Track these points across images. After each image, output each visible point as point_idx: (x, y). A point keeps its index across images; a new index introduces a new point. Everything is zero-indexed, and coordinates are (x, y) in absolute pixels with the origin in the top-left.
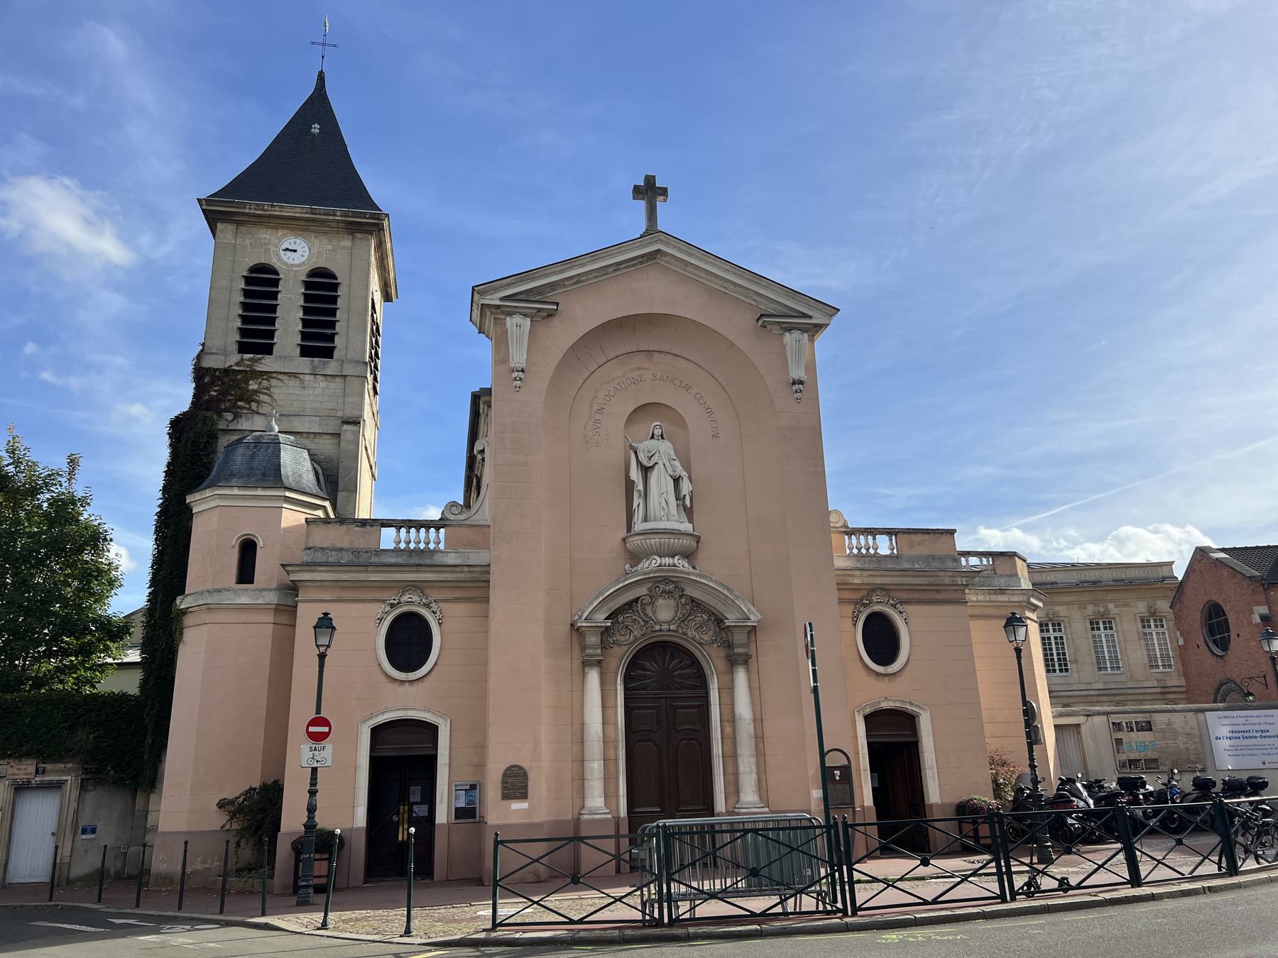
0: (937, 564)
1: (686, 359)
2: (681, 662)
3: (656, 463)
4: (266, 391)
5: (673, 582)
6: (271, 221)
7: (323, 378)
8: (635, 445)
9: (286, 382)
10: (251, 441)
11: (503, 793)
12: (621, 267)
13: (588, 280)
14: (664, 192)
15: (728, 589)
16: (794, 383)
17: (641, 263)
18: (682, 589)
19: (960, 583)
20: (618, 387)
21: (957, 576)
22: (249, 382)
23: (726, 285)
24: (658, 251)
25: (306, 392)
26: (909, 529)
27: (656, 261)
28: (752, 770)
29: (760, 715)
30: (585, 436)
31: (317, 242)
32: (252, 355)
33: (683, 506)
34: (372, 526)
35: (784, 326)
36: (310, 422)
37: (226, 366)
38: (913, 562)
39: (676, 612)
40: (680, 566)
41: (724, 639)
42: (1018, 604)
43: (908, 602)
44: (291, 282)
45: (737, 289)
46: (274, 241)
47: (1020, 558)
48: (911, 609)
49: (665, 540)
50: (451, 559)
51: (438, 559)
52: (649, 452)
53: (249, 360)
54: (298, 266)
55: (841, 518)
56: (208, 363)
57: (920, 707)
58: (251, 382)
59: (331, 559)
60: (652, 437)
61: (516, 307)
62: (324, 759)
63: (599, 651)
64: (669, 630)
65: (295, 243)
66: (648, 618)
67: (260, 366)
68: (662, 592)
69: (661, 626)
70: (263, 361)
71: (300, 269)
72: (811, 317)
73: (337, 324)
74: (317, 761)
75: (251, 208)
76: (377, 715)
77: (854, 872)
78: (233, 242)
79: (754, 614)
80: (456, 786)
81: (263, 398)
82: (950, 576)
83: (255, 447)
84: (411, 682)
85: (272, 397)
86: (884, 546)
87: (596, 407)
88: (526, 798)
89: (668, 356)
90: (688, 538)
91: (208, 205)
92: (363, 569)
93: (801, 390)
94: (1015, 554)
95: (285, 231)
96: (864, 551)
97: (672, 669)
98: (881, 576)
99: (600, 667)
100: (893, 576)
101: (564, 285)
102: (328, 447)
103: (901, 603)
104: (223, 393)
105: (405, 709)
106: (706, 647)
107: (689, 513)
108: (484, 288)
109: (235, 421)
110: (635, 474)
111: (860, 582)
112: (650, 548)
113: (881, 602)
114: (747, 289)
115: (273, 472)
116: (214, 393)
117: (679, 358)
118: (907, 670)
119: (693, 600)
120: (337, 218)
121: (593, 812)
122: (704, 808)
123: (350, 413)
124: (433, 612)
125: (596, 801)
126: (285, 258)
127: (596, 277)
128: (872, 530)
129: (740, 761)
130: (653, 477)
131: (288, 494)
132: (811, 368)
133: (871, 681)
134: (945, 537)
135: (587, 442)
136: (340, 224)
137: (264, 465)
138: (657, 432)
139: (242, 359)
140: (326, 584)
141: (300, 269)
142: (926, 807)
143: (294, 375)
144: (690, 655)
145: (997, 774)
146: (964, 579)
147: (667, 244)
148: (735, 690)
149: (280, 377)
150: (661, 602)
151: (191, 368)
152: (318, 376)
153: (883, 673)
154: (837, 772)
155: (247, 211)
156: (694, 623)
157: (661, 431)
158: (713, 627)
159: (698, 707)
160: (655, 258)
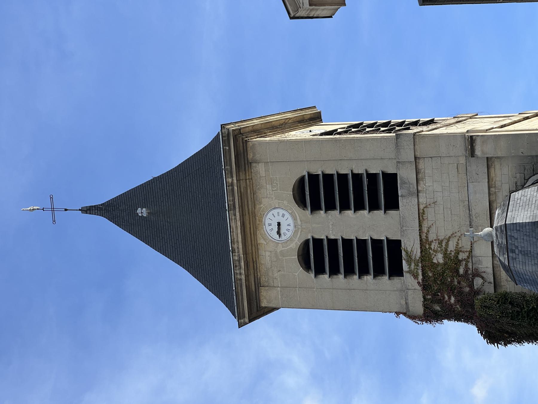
4: (444, 244)
7: (421, 182)
9: (430, 224)
10: (506, 256)
22: (435, 263)
31: (265, 201)
32: (404, 262)
37: (419, 288)
53: (410, 265)
54: (295, 219)
56: (418, 308)
58: (435, 261)
70: (409, 250)
71: (298, 217)
73: (356, 171)
81: (452, 247)
83: (513, 251)
85: (450, 237)
91: (244, 317)
95: (259, 236)
108: (290, 4)
109: (484, 275)
116: (453, 300)
120: (235, 181)
123: (460, 149)
126: (289, 234)
139: (409, 272)
141: (298, 217)
149: (425, 230)
151: (427, 326)
152: (420, 188)
155: (243, 277)
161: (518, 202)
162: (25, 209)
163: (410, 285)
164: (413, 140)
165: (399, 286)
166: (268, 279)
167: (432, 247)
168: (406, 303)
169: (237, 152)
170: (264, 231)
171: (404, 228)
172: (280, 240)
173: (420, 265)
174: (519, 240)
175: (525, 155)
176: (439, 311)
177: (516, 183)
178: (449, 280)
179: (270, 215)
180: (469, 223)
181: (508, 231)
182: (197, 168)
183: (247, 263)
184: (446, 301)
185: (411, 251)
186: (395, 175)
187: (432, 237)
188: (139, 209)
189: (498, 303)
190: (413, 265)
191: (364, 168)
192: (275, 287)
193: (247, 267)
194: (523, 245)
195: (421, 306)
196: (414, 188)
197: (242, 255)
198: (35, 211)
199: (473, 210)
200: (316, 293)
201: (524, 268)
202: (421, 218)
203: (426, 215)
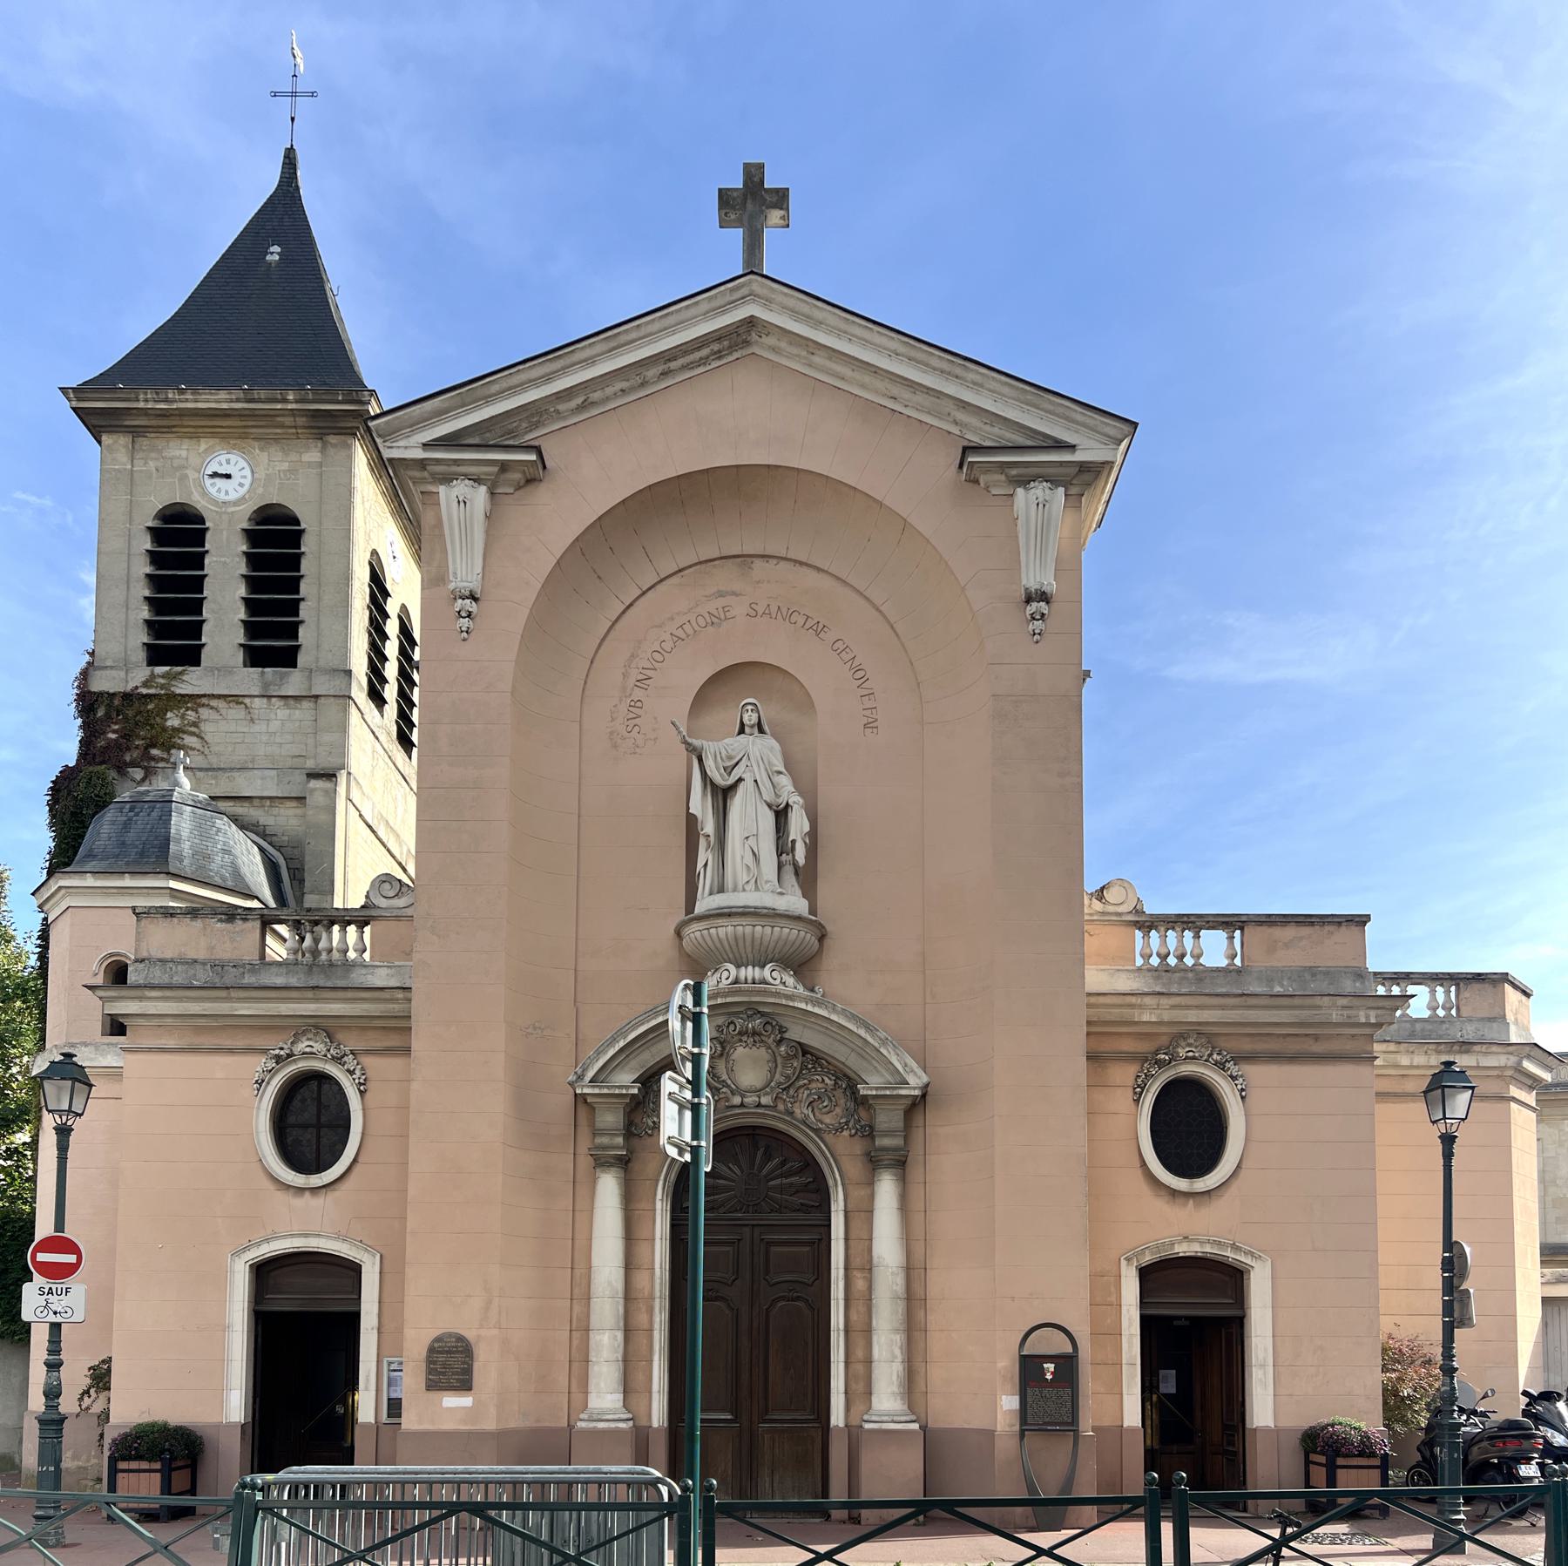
0: (1322, 986)
1: (819, 569)
2: (783, 1163)
3: (740, 780)
4: (193, 729)
5: (763, 1014)
6: (186, 423)
7: (282, 703)
8: (696, 742)
9: (223, 712)
10: (126, 799)
11: (428, 1380)
12: (673, 365)
13: (608, 399)
14: (780, 198)
15: (867, 1027)
16: (1028, 600)
17: (719, 355)
18: (781, 1027)
19: (1363, 1020)
20: (680, 633)
21: (1358, 1008)
22: (166, 714)
23: (895, 390)
24: (751, 322)
25: (256, 728)
26: (1270, 915)
27: (750, 351)
28: (895, 1357)
29: (922, 1259)
30: (611, 733)
31: (264, 457)
32: (168, 668)
33: (794, 864)
34: (245, 920)
35: (1014, 472)
36: (262, 779)
37: (129, 688)
38: (1270, 981)
39: (773, 1072)
40: (778, 982)
41: (863, 1123)
42: (1495, 1073)
43: (1251, 1058)
44: (225, 533)
45: (919, 398)
46: (194, 460)
47: (1515, 987)
48: (1253, 1071)
49: (744, 928)
50: (380, 978)
51: (358, 977)
52: (730, 758)
53: (163, 677)
54: (236, 503)
55: (1130, 895)
56: (100, 684)
57: (1252, 1254)
58: (169, 715)
59: (177, 980)
60: (742, 731)
61: (456, 462)
62: (68, 1310)
63: (620, 1140)
64: (759, 1105)
65: (228, 462)
66: (719, 1082)
67: (180, 685)
68: (740, 1033)
69: (743, 1096)
70: (185, 678)
71: (237, 508)
72: (1072, 448)
73: (302, 605)
74: (55, 1313)
75: (146, 401)
76: (258, 1244)
77: (1054, 1552)
78: (129, 467)
79: (915, 1074)
80: (390, 1363)
81: (189, 740)
82: (1344, 1007)
83: (131, 810)
84: (314, 1190)
85: (202, 738)
86: (1215, 949)
87: (635, 675)
88: (470, 1389)
89: (782, 564)
90: (792, 924)
91: (79, 399)
92: (223, 993)
93: (1043, 615)
94: (1504, 978)
95: (212, 442)
96: (1172, 961)
97: (765, 1177)
98: (1197, 1007)
99: (626, 1171)
100: (1223, 1007)
101: (558, 412)
102: (294, 822)
103: (1237, 1060)
104: (127, 736)
105: (306, 1236)
106: (829, 1138)
107: (807, 878)
108: (387, 422)
109: (147, 782)
110: (700, 804)
111: (1154, 1019)
112: (718, 945)
113: (1194, 1058)
114: (939, 394)
115: (156, 850)
116: (113, 736)
117: (805, 569)
118: (1234, 1189)
119: (805, 1050)
120: (290, 406)
121: (595, 1417)
122: (812, 1417)
123: (324, 762)
124: (348, 1071)
125: (605, 1398)
126: (213, 491)
127: (622, 391)
128: (1192, 919)
129: (875, 1338)
130: (736, 805)
131: (173, 884)
132: (1069, 567)
133: (1161, 1205)
134: (1345, 933)
135: (615, 746)
136: (297, 419)
137: (144, 839)
138: (750, 718)
139: (153, 676)
140: (169, 1021)
141: (237, 508)
142: (1247, 1432)
143: (234, 699)
144: (803, 1151)
145: (1400, 1379)
146: (1372, 1013)
147: (767, 302)
148: (875, 1212)
149: (214, 703)
150: (740, 1052)
151: (72, 693)
152: (274, 700)
153: (1186, 1190)
154: (1050, 1367)
155: (141, 405)
156: (806, 1092)
157: (755, 715)
158: (842, 1102)
159: (811, 1243)
160: (747, 343)
161: (208, 823)
162: (294, 38)
163: (134, 675)
164: (341, 694)
165: (134, 659)
166: (144, 451)
167: (189, 712)
168: (106, 667)
169: (335, 416)
170: (219, 450)
171: (216, 672)
172: (205, 476)
173: (163, 692)
174: (146, 818)
175: (306, 846)
176: (95, 714)
177: (275, 835)
178: (141, 733)
179: (242, 463)
180: (222, 766)
181: (162, 804)
182: (323, 350)
183: (165, 416)
184: (109, 726)
185: (184, 681)
186: (295, 666)
187: (205, 713)
188: (279, 250)
189: (96, 796)
190: (162, 681)
191: (306, 619)
192: (132, 461)
193: (160, 415)
194: (139, 823)
195: (101, 689)
196: (274, 691)
197: (175, 407)
198: (292, 58)
199: (238, 774)
200: (123, 527)
201: (105, 823)
202: (231, 699)
203: (236, 706)
